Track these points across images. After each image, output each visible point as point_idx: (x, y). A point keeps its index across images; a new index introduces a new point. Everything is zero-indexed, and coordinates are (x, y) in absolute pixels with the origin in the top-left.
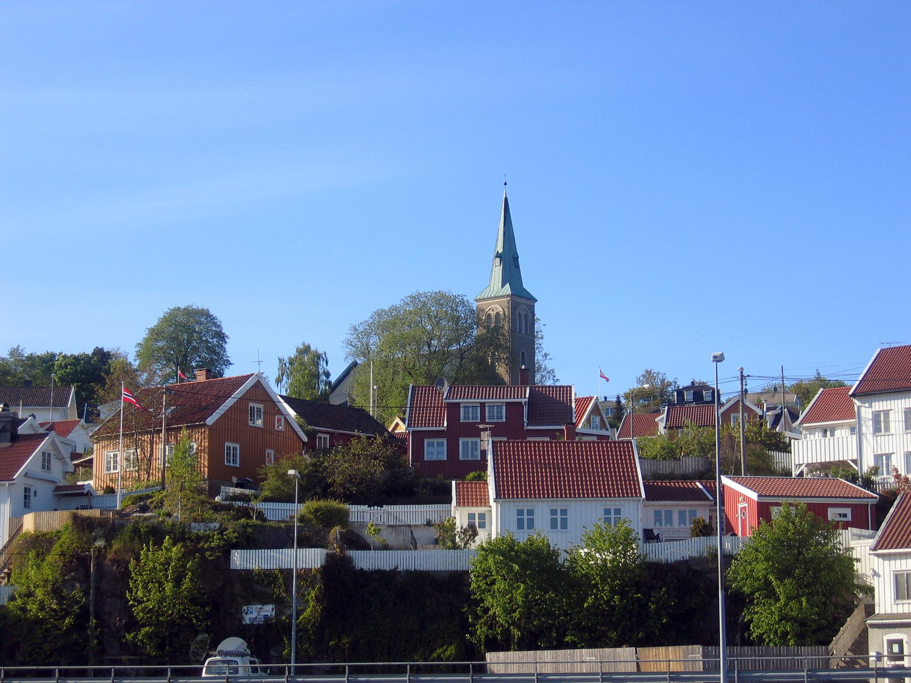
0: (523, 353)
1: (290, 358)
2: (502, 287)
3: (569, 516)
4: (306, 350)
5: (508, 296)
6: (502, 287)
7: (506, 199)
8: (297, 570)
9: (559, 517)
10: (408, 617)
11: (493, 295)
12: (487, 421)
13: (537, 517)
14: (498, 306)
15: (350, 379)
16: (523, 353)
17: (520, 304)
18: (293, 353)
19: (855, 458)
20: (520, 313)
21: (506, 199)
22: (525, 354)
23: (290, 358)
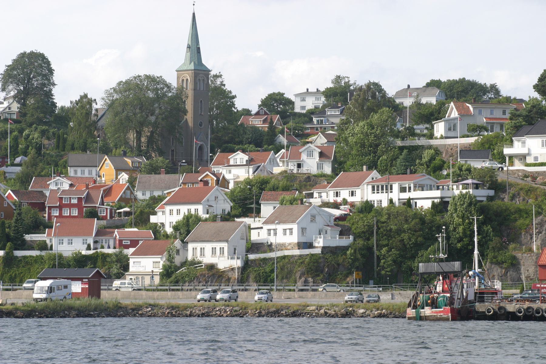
0: (201, 101)
1: (76, 101)
2: (190, 64)
3: (356, 192)
4: (86, 96)
5: (192, 70)
6: (190, 64)
7: (194, 14)
8: (508, 183)
9: (61, 241)
10: (197, 360)
11: (185, 69)
12: (105, 215)
13: (64, 241)
14: (187, 75)
15: (104, 117)
16: (201, 101)
17: (199, 74)
18: (78, 98)
19: (272, 208)
20: (199, 79)
21: (194, 14)
22: (203, 102)
23: (76, 101)
